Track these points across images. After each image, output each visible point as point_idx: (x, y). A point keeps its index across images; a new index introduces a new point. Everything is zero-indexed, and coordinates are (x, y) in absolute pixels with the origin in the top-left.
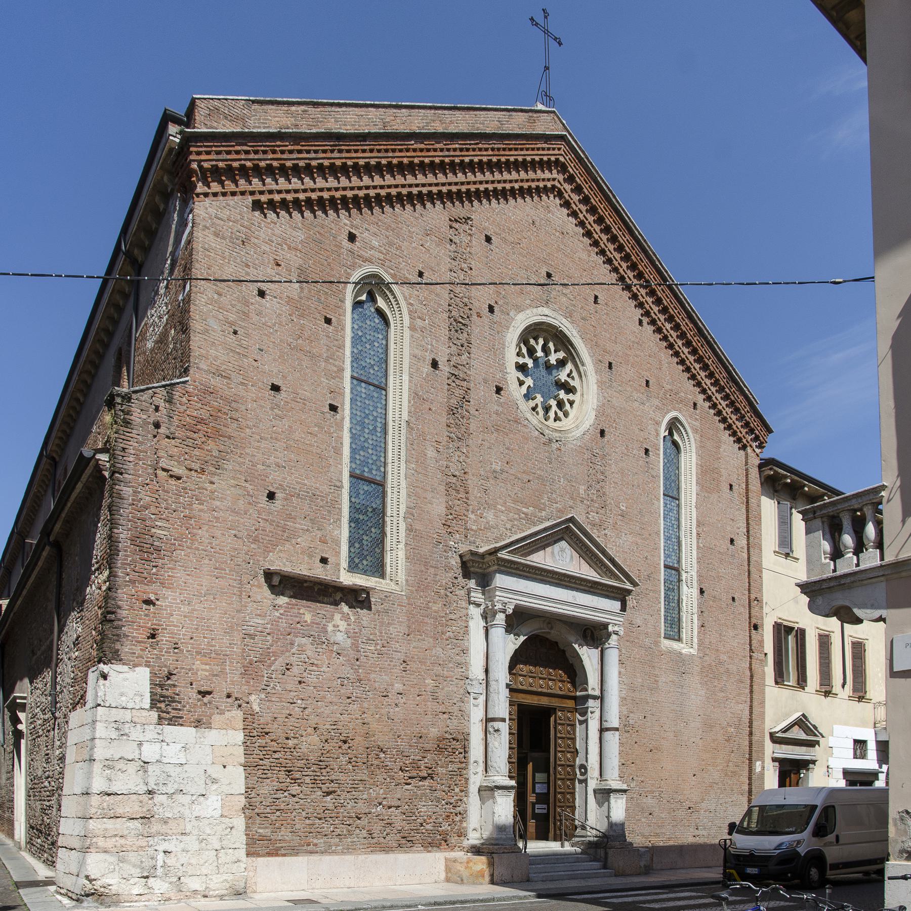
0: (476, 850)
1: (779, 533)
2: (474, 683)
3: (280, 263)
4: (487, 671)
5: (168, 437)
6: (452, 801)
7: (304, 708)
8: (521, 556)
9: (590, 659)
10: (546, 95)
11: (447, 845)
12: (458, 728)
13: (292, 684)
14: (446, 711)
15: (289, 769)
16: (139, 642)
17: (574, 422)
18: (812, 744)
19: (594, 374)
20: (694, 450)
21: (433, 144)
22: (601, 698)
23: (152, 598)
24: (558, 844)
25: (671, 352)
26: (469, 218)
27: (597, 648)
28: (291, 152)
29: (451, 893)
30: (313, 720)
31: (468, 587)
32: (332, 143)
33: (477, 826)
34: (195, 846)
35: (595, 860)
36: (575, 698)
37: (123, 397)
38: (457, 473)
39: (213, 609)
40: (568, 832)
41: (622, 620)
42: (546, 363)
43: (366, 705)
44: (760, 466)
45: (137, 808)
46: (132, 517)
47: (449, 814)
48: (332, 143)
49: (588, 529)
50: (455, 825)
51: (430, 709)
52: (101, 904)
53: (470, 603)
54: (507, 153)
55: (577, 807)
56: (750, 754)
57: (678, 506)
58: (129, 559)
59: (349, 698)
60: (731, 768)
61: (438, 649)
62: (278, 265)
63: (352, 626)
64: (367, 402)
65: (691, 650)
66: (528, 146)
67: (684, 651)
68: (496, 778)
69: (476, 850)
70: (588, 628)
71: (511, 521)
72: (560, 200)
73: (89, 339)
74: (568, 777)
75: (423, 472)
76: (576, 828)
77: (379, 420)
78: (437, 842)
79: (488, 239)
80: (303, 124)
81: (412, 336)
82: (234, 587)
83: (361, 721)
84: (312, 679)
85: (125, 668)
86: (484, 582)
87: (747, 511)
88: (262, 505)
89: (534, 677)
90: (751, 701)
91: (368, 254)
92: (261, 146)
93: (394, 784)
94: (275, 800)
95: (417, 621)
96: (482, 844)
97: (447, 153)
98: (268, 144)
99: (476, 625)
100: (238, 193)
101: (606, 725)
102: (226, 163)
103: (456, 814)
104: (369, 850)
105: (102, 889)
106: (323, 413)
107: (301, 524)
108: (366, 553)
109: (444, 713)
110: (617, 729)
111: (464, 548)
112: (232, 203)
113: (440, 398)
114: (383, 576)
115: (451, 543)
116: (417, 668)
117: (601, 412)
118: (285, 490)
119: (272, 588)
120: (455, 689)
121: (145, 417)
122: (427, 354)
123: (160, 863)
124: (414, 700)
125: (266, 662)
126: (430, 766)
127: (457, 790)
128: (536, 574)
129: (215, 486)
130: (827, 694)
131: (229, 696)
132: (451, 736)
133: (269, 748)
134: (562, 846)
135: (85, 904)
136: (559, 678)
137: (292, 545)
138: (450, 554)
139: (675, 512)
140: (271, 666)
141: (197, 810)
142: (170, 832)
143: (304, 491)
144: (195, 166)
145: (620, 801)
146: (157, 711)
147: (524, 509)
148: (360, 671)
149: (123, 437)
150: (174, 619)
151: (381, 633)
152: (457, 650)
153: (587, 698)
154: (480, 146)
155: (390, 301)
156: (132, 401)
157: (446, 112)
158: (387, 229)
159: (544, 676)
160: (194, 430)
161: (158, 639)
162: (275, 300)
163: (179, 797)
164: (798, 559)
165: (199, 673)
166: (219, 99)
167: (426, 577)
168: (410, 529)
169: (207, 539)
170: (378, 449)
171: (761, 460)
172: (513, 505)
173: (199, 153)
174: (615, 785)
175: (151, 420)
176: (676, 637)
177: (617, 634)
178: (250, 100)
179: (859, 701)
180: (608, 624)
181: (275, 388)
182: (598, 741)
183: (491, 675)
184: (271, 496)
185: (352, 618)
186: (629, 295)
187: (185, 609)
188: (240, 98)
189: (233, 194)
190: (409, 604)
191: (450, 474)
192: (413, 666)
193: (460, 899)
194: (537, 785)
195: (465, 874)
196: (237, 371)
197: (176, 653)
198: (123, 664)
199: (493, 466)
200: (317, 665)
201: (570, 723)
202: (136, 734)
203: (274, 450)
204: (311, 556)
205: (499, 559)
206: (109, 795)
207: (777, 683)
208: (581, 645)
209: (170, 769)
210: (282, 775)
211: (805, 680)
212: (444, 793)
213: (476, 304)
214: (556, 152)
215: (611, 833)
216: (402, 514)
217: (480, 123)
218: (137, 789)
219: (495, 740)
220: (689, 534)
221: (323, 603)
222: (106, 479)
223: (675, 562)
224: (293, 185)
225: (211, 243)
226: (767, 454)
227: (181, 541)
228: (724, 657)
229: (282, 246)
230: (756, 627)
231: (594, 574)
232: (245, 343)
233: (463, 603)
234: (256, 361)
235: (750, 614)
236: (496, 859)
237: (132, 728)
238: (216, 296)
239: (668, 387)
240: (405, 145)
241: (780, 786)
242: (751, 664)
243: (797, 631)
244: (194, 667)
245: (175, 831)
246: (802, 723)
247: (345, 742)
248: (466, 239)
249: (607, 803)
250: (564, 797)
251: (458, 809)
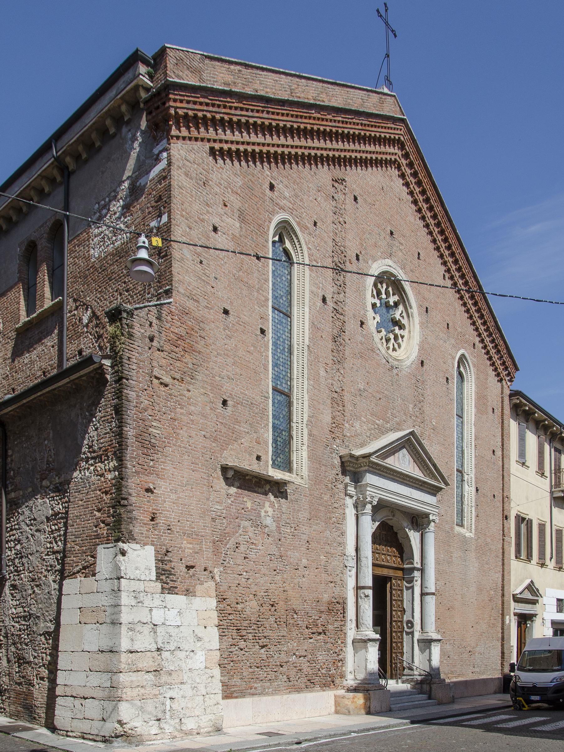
0: (356, 690)
1: (519, 447)
3: (227, 204)
5: (159, 350)
6: (337, 651)
7: (248, 579)
10: (387, 80)
13: (240, 561)
15: (239, 628)
16: (145, 524)
17: (405, 354)
18: (534, 602)
19: (417, 316)
20: (473, 381)
21: (326, 115)
22: (422, 570)
23: (152, 487)
25: (461, 302)
26: (344, 180)
27: (419, 532)
28: (236, 108)
30: (254, 588)
32: (263, 105)
34: (189, 693)
35: (421, 693)
36: (402, 569)
37: (128, 313)
38: (338, 390)
39: (191, 497)
41: (437, 511)
42: (386, 303)
43: (285, 576)
44: (511, 396)
45: (151, 663)
46: (136, 417)
48: (263, 105)
52: (129, 743)
53: (346, 495)
54: (370, 129)
55: (405, 653)
56: (503, 611)
58: (135, 453)
59: (275, 570)
60: (492, 621)
62: (226, 206)
63: (276, 512)
64: (279, 326)
65: (471, 534)
66: (382, 125)
68: (367, 633)
69: (356, 690)
72: (398, 171)
75: (318, 388)
76: (404, 669)
77: (286, 342)
79: (355, 199)
80: (239, 83)
81: (310, 275)
82: (204, 479)
83: (283, 589)
84: (252, 556)
85: (137, 546)
86: (357, 478)
87: (502, 429)
88: (219, 411)
90: (503, 571)
91: (283, 202)
92: (216, 100)
93: (302, 638)
94: (230, 653)
95: (315, 508)
97: (334, 124)
98: (222, 99)
99: (350, 512)
100: (200, 139)
101: (361, 584)
102: (194, 112)
104: (288, 691)
105: (130, 731)
106: (256, 335)
107: (244, 428)
108: (279, 452)
110: (433, 594)
111: (343, 451)
112: (195, 147)
113: (328, 329)
114: (290, 470)
116: (315, 547)
117: (422, 348)
118: (233, 399)
119: (226, 479)
120: (338, 563)
121: (143, 331)
122: (320, 291)
123: (168, 708)
124: (314, 572)
125: (223, 541)
127: (339, 642)
128: (390, 474)
129: (190, 393)
130: (543, 565)
131: (205, 570)
133: (226, 612)
134: (397, 683)
135: (115, 744)
137: (238, 444)
138: (334, 455)
140: (226, 545)
141: (191, 664)
142: (173, 682)
143: (245, 400)
144: (172, 111)
145: (436, 648)
146: (161, 582)
148: (282, 549)
149: (128, 347)
150: (167, 505)
151: (294, 518)
154: (354, 120)
155: (295, 244)
156: (134, 316)
157: (329, 86)
158: (294, 183)
159: (384, 552)
160: (176, 345)
161: (157, 521)
162: (224, 236)
163: (178, 653)
164: (529, 467)
165: (186, 550)
166: (183, 51)
167: (320, 473)
168: (310, 435)
169: (186, 438)
170: (286, 366)
171: (511, 391)
172: (371, 418)
173: (175, 101)
174: (435, 636)
175: (147, 334)
177: (434, 522)
178: (203, 55)
179: (559, 571)
180: (429, 514)
181: (226, 312)
184: (225, 403)
185: (276, 505)
186: (438, 254)
187: (173, 496)
188: (197, 52)
189: (196, 139)
190: (310, 495)
191: (333, 390)
192: (313, 545)
195: (351, 707)
196: (204, 296)
197: (170, 534)
198: (137, 543)
199: (359, 386)
200: (255, 544)
202: (148, 602)
203: (226, 364)
204: (250, 454)
206: (132, 652)
207: (516, 557)
209: (171, 630)
210: (234, 633)
211: (532, 556)
213: (349, 252)
214: (398, 132)
216: (305, 422)
217: (350, 99)
218: (150, 647)
220: (469, 446)
221: (258, 493)
222: (108, 382)
224: (235, 137)
225: (183, 182)
226: (516, 386)
227: (169, 439)
228: (489, 540)
229: (227, 189)
230: (506, 518)
231: (422, 475)
232: (208, 272)
233: (342, 495)
234: (213, 287)
235: (503, 507)
236: (372, 695)
237: (145, 597)
238: (188, 229)
239: (460, 330)
240: (308, 113)
241: (553, 636)
242: (503, 545)
243: (528, 521)
244: (183, 546)
245: (176, 681)
246: (531, 588)
247: (272, 606)
248: (342, 197)
249: (428, 650)
250: (397, 645)
251: (340, 657)
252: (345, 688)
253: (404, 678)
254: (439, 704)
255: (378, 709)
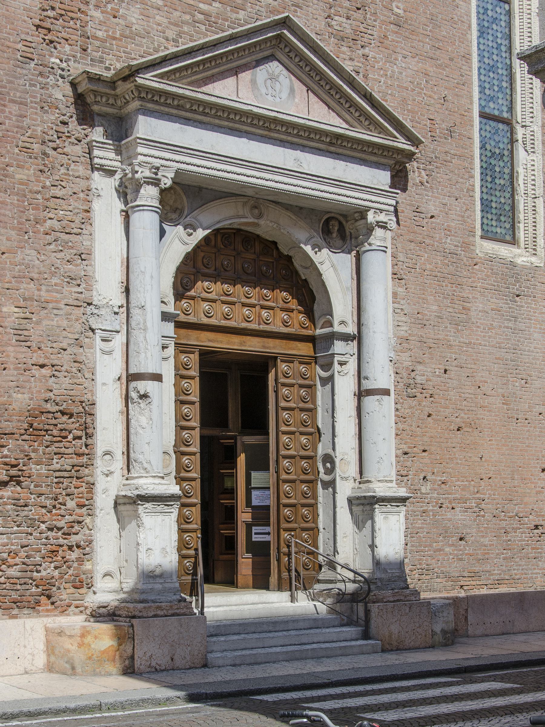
2: (103, 312)
4: (127, 291)
6: (61, 524)
8: (189, 84)
9: (335, 270)
11: (53, 603)
12: (72, 393)
14: (46, 361)
24: (286, 595)
27: (349, 253)
29: (27, 695)
31: (88, 139)
33: (113, 568)
36: (312, 339)
40: (302, 572)
47: (54, 548)
49: (329, 48)
50: (69, 567)
51: (12, 359)
53: (93, 168)
55: (321, 530)
57: (509, 13)
61: (28, 252)
65: (533, 259)
67: (519, 261)
70: (333, 218)
71: (176, 25)
73: (340, 164)
74: (303, 477)
76: (320, 567)
78: (31, 599)
89: (233, 303)
96: (124, 601)
101: (367, 385)
103: (70, 548)
109: (42, 366)
115: (53, 60)
120: (65, 323)
126: (13, 461)
127: (71, 504)
132: (57, 408)
134: (293, 599)
136: (281, 304)
138: (51, 80)
139: (503, 24)
145: (393, 518)
147: (201, 5)
152: (67, 254)
153: (332, 337)
176: (508, 238)
177: (385, 228)
182: (354, 413)
183: (132, 296)
193: (25, 709)
194: (254, 493)
195: (79, 656)
201: (307, 382)
205: (139, 88)
208: (317, 247)
212: (44, 511)
215: (378, 575)
219: (140, 413)
223: (505, 109)
231: (338, 121)
249: (370, 522)
251: (74, 539)
252: (88, 612)
253: (318, 587)
254: (383, 651)
255: (163, 661)
